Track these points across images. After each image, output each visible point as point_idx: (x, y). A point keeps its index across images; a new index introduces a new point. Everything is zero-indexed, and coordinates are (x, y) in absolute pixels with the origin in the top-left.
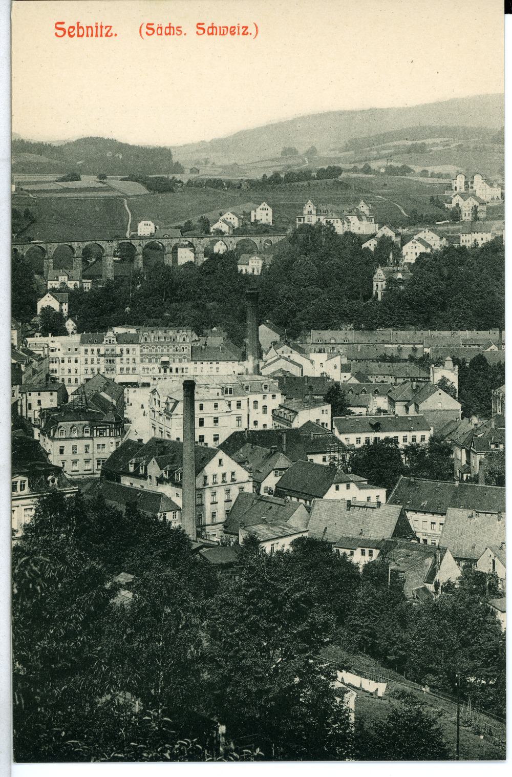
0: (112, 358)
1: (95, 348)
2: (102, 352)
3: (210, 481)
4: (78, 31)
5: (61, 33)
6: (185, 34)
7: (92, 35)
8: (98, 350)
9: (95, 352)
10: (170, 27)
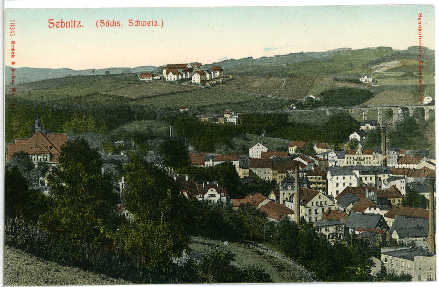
0: (359, 161)
1: (352, 156)
2: (355, 158)
3: (315, 204)
4: (61, 24)
5: (51, 25)
6: (122, 26)
7: (69, 27)
8: (353, 158)
9: (352, 158)
10: (113, 22)
